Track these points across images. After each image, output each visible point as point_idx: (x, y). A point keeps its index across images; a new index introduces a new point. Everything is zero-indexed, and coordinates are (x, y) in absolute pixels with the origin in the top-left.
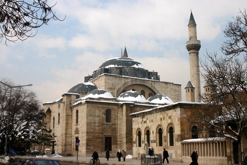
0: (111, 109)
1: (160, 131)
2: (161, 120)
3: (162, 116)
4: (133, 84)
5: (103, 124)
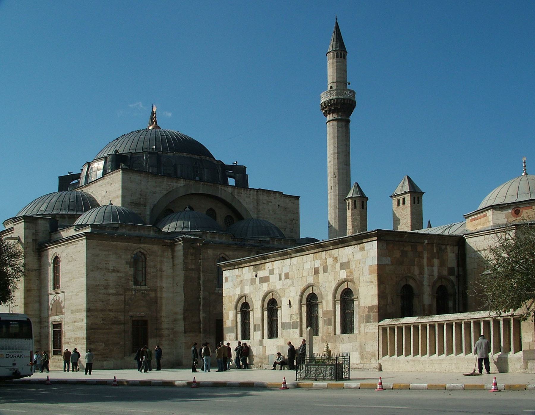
0: (145, 253)
1: (311, 302)
2: (316, 271)
3: (317, 264)
4: (189, 193)
5: (126, 290)
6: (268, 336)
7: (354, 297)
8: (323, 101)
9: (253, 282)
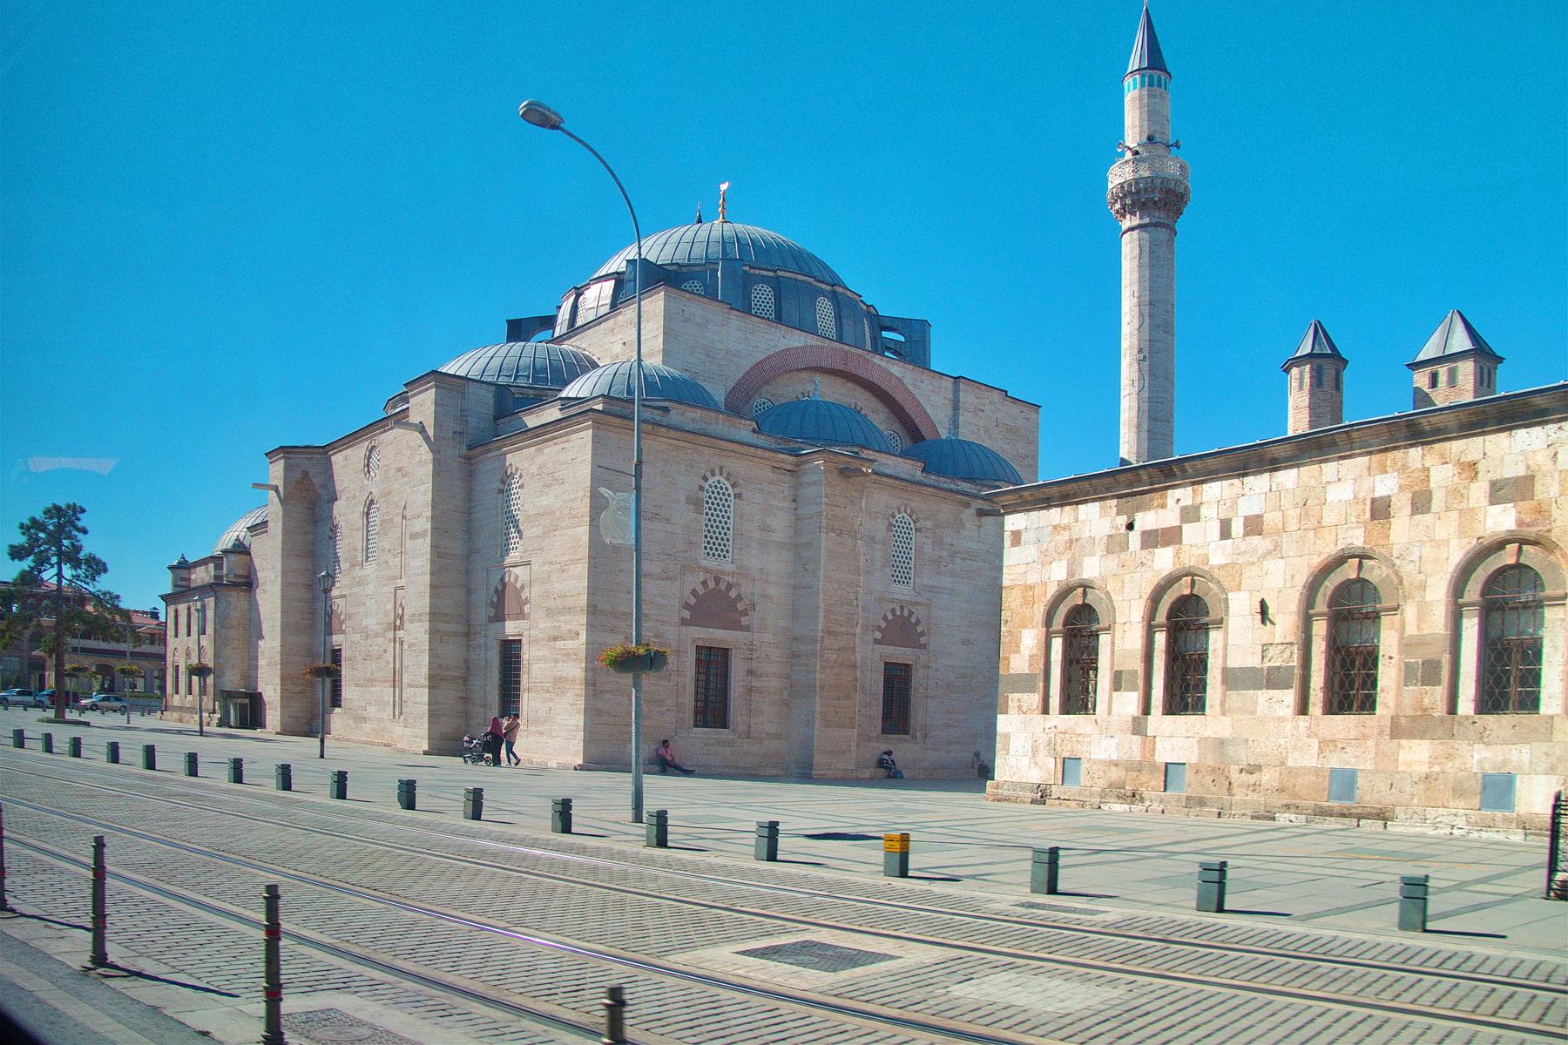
3: (1386, 485)
6: (1324, 706)
7: (1548, 592)
8: (1117, 182)
9: (1115, 545)
